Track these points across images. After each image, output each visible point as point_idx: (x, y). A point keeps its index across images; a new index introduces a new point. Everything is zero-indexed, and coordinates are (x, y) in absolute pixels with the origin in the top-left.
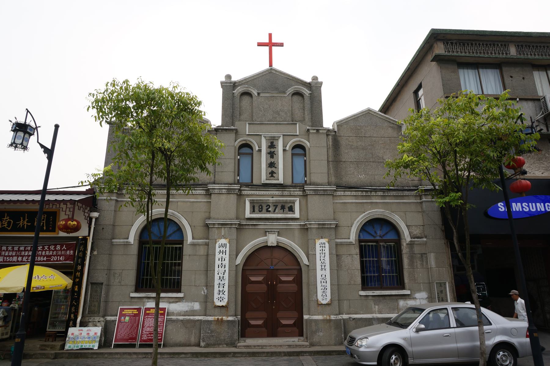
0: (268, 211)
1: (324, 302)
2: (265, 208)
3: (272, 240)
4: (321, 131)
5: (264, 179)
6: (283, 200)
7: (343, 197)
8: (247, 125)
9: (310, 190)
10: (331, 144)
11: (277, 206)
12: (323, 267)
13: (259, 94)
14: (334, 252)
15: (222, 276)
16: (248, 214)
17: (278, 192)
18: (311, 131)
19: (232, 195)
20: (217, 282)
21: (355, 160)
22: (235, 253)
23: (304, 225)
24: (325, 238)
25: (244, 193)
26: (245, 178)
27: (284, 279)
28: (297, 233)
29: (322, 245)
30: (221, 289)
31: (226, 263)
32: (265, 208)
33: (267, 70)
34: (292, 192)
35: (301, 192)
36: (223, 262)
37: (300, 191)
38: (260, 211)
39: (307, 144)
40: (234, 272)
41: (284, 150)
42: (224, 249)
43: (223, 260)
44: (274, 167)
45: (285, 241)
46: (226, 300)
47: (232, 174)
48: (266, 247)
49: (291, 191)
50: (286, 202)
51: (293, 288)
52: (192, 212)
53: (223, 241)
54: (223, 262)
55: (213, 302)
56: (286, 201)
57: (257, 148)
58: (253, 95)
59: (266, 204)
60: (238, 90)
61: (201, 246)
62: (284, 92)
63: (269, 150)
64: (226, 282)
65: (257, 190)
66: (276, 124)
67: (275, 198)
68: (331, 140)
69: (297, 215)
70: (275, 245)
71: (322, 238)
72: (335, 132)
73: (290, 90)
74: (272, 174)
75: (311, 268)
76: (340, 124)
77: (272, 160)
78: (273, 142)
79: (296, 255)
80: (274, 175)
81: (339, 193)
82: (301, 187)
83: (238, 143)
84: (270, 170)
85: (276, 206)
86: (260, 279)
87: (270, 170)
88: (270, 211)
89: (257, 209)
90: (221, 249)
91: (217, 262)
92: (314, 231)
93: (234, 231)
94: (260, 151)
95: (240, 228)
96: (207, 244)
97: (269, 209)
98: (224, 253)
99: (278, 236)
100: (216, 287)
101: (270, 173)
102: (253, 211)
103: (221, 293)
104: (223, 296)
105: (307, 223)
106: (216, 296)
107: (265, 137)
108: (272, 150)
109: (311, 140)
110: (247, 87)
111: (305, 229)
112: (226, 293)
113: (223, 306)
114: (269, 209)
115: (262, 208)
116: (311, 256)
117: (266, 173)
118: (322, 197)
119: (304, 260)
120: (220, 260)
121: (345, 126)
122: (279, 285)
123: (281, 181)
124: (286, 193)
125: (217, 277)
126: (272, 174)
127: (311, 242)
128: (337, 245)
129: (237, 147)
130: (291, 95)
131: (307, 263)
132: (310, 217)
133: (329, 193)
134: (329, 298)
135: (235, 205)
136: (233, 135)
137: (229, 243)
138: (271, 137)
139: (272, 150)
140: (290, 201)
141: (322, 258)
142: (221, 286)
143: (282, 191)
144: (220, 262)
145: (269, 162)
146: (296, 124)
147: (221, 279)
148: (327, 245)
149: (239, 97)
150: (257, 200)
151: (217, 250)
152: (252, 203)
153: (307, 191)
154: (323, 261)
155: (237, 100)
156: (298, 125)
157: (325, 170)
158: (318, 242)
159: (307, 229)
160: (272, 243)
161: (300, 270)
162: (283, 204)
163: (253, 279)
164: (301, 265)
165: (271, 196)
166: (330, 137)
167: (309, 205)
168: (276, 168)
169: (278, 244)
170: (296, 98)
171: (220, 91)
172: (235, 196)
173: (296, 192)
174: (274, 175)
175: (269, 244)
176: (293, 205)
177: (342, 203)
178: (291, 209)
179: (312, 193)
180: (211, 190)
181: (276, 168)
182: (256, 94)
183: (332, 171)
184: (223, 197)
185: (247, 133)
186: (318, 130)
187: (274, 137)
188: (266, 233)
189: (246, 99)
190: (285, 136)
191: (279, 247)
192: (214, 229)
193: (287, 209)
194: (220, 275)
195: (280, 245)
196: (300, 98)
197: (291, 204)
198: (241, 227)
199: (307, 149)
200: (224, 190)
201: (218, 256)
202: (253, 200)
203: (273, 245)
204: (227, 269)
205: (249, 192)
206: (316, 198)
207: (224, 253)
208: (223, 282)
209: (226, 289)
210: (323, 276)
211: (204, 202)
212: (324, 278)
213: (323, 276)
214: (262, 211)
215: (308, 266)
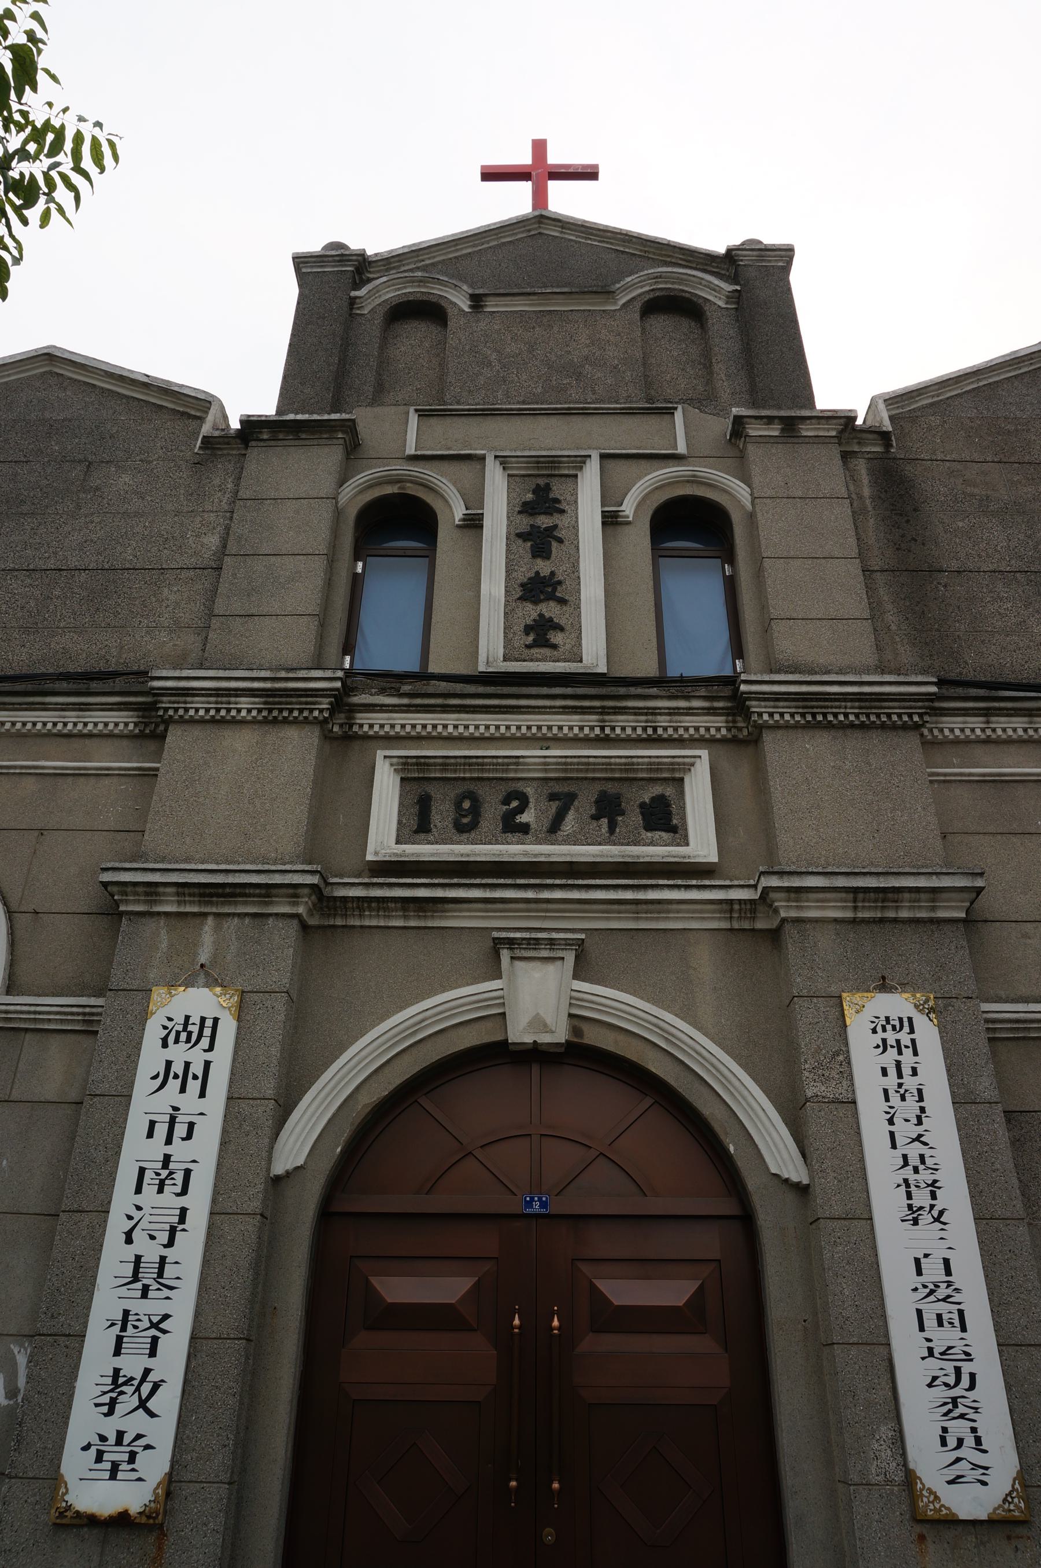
0: (513, 827)
1: (971, 1503)
2: (492, 811)
3: (538, 1000)
4: (807, 431)
5: (491, 650)
6: (607, 765)
7: (979, 751)
8: (413, 419)
9: (777, 697)
10: (866, 492)
11: (571, 797)
12: (922, 1198)
13: (477, 301)
14: (985, 1086)
15: (151, 1253)
16: (383, 836)
17: (575, 720)
18: (755, 430)
19: (292, 733)
20: (108, 1300)
21: (1016, 564)
22: (269, 1087)
23: (750, 908)
24: (904, 986)
25: (369, 722)
26: (388, 645)
27: (624, 1292)
28: (705, 962)
29: (894, 1035)
30: (132, 1365)
31: (202, 1152)
32: (492, 811)
33: (520, 223)
34: (663, 721)
35: (719, 721)
36: (180, 1151)
37: (710, 711)
38: (466, 825)
39: (735, 492)
40: (250, 1226)
41: (611, 520)
42: (197, 1057)
43: (180, 1130)
44: (551, 597)
45: (630, 1011)
46: (155, 1466)
47: (308, 628)
48: (494, 1056)
49: (654, 712)
50: (628, 775)
51: (694, 1366)
52: (41, 832)
53: (199, 1001)
54: (180, 1151)
55: (56, 1480)
56: (629, 766)
57: (459, 511)
58: (451, 312)
59: (503, 789)
60: (377, 295)
61: (55, 1043)
62: (607, 293)
63: (524, 523)
64: (181, 1308)
65: (445, 709)
66: (568, 413)
67: (554, 781)
68: (865, 479)
69: (702, 843)
70: (560, 1034)
71: (884, 986)
72: (885, 436)
73: (635, 286)
74: (541, 634)
75: (833, 1207)
76: (906, 404)
77: (544, 567)
78: (548, 488)
79: (708, 1109)
80: (557, 638)
81: (953, 726)
82: (727, 693)
83: (354, 494)
84: (530, 612)
85: (564, 802)
86: (448, 1288)
87: (530, 612)
88: (525, 829)
89: (442, 815)
90: (178, 1053)
91: (138, 1149)
92: (825, 941)
93: (282, 944)
94: (474, 523)
95: (327, 917)
96: (88, 1027)
97: (525, 818)
98: (194, 1086)
99: (576, 976)
100: (98, 1340)
101: (528, 629)
102: (418, 821)
103: (128, 1401)
104: (138, 1422)
105: (774, 882)
106: (85, 1421)
107: (503, 461)
108: (544, 521)
109: (755, 470)
110: (422, 281)
111: (759, 932)
112: (168, 1402)
113: (122, 1519)
114: (525, 818)
115: (476, 811)
116: (819, 1110)
117: (507, 628)
118: (854, 742)
119: (777, 1151)
120: (161, 1130)
121: (935, 420)
122: (591, 1343)
123: (594, 653)
124: (625, 724)
125: (114, 1259)
126: (541, 634)
127: (806, 1014)
128: (1003, 1038)
129: (352, 513)
130: (638, 305)
131: (795, 1171)
132: (789, 854)
133: (896, 713)
134: (1003, 1462)
135: (306, 785)
136: (328, 457)
137: (241, 1013)
138: (538, 461)
139: (544, 521)
140: (655, 766)
141: (905, 1130)
142: (137, 1340)
143: (603, 711)
144: (156, 1148)
145: (524, 573)
146: (670, 412)
147: (148, 1277)
148: (927, 1032)
149: (378, 321)
150: (445, 763)
151: (151, 1057)
152: (416, 779)
153: (755, 707)
154: (914, 1151)
155: (371, 331)
156: (678, 416)
157: (855, 604)
158: (867, 1013)
159: (774, 936)
160: (538, 1023)
161: (746, 1220)
162: (611, 788)
163: (399, 1289)
164: (753, 1182)
165: (539, 742)
166: (861, 467)
167: (776, 785)
168: (562, 601)
169: (576, 1031)
170: (660, 324)
171: (287, 292)
172: (312, 737)
173: (688, 721)
174: (557, 638)
175: (520, 1033)
176: (669, 791)
177: (984, 781)
178: (663, 818)
179: (787, 714)
180: (165, 702)
181: (562, 601)
182: (465, 305)
183: (891, 618)
184: (240, 742)
185: (411, 450)
186: (790, 425)
187: (553, 461)
188: (495, 953)
189: (415, 336)
190: (611, 464)
191: (582, 1056)
192: (151, 924)
193: (634, 818)
194: (142, 1245)
195: (593, 1037)
196: (686, 324)
197: (657, 790)
198: (332, 916)
199: (736, 517)
200: (245, 703)
201: (146, 1102)
202: (422, 763)
203: (545, 1039)
204: (199, 1201)
205: (399, 719)
206: (818, 747)
207: (194, 1086)
208: (154, 1307)
209: (172, 1361)
210: (933, 1271)
211: (124, 774)
212: (942, 1289)
213: (933, 1271)
214: (473, 826)
215: (802, 1190)
